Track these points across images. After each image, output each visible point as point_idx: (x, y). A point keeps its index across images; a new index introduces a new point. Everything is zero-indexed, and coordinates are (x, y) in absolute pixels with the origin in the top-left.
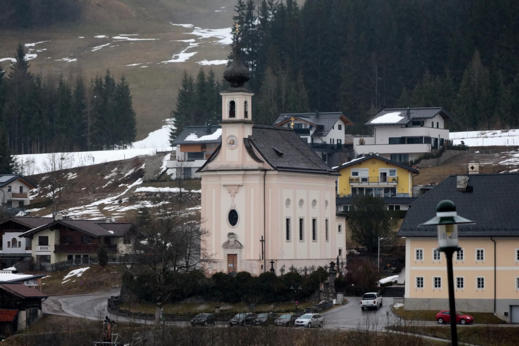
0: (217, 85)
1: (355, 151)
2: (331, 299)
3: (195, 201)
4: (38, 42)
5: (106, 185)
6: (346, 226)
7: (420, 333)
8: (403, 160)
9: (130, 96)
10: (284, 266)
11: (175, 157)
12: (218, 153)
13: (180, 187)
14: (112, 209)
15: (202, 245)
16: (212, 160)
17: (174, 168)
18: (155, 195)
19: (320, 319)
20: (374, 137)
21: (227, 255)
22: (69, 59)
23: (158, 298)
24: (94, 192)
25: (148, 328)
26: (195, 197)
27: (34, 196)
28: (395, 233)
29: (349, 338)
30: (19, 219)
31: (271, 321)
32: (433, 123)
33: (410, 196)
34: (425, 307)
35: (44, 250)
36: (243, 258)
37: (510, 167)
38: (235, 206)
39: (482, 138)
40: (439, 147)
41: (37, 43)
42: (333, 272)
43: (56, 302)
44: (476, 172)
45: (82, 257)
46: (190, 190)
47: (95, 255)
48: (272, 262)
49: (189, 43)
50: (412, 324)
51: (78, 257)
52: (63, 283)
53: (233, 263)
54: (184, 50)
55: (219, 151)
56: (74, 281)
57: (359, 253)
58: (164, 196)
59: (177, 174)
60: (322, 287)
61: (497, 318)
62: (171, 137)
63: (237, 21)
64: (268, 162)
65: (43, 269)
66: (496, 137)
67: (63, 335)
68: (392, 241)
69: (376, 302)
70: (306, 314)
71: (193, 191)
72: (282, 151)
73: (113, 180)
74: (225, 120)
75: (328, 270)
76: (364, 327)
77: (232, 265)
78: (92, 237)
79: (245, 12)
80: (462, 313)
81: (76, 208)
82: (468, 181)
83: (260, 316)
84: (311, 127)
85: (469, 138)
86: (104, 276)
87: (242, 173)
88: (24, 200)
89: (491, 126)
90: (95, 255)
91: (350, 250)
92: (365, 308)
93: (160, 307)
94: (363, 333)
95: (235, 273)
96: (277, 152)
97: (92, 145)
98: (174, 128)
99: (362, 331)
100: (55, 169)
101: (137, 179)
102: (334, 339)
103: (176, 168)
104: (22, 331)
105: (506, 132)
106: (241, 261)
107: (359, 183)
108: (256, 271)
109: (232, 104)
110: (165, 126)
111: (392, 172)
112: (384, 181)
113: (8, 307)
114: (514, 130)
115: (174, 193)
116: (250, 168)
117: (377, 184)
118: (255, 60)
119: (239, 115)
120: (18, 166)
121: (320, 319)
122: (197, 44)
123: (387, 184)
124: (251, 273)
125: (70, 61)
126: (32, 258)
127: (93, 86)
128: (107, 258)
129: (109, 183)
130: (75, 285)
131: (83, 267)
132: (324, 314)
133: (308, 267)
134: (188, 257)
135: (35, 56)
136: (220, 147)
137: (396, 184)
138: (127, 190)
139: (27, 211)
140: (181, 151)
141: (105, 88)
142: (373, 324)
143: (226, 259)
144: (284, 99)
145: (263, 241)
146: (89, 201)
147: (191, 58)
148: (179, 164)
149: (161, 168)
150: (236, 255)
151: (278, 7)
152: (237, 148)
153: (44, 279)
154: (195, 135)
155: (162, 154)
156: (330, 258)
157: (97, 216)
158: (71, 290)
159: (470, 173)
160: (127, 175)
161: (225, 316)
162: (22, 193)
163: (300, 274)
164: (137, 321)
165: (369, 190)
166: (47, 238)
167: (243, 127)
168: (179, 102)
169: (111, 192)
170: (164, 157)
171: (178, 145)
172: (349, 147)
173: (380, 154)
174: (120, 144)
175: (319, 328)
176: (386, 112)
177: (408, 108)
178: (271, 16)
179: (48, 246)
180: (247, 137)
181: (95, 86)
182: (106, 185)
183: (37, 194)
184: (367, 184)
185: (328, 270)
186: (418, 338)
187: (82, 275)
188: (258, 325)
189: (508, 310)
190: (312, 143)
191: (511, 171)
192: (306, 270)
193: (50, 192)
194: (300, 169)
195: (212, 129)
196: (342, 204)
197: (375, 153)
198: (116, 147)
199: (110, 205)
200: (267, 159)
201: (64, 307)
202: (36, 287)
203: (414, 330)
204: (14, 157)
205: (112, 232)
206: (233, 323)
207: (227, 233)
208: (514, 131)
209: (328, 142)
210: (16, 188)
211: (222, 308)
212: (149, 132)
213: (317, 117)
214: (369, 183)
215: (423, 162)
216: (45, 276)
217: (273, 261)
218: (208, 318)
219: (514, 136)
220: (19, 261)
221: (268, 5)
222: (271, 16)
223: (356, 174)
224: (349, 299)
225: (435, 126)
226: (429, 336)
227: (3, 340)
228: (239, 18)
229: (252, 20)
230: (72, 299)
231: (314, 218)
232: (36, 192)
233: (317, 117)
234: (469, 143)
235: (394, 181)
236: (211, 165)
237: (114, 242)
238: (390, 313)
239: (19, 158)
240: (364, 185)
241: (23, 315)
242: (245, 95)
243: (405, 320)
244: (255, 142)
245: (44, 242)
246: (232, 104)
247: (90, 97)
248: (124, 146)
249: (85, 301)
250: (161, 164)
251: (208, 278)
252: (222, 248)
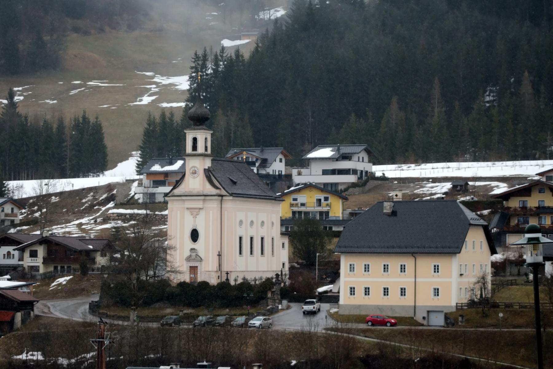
0: (176, 123)
1: (294, 181)
2: (277, 305)
3: (158, 221)
4: (24, 86)
5: (84, 207)
6: (289, 244)
7: (353, 334)
8: (334, 189)
9: (102, 132)
10: (238, 276)
11: (142, 184)
12: (182, 181)
13: (146, 209)
14: (89, 227)
15: (168, 258)
16: (178, 187)
17: (141, 193)
18: (125, 216)
19: (270, 321)
20: (310, 169)
21: (189, 267)
22: (50, 100)
23: (133, 303)
24: (74, 213)
25: (124, 328)
26: (158, 218)
27: (23, 216)
28: (330, 250)
29: (294, 337)
30: (12, 235)
31: (228, 322)
32: (359, 157)
33: (341, 219)
34: (356, 312)
35: (34, 261)
36: (203, 270)
37: (424, 195)
38: (196, 226)
39: (400, 171)
40: (364, 178)
41: (23, 87)
42: (278, 282)
43: (45, 306)
44: (400, 199)
45: (66, 267)
46: (155, 212)
47: (77, 266)
48: (227, 273)
49: (151, 88)
50: (347, 326)
51: (62, 267)
52: (50, 289)
53: (194, 274)
54: (147, 94)
55: (183, 180)
56: (60, 288)
57: (299, 266)
58: (132, 217)
59: (143, 198)
60: (269, 295)
61: (416, 321)
62: (138, 167)
63: (193, 70)
64: (224, 188)
65: (33, 278)
66: (410, 170)
67: (54, 333)
68: (327, 256)
69: (315, 307)
70: (258, 317)
71: (157, 213)
72: (236, 179)
73: (89, 203)
74: (189, 153)
75: (274, 280)
76: (307, 329)
77: (193, 276)
78: (75, 251)
79: (200, 63)
80: (387, 316)
81: (59, 226)
82: (393, 206)
83: (219, 318)
84: (257, 160)
85: (388, 170)
86: (84, 284)
87: (203, 198)
88: (14, 219)
89: (406, 161)
90: (77, 266)
91: (292, 264)
92: (306, 313)
93: (134, 310)
94: (307, 334)
95: (196, 282)
96: (232, 180)
97: (70, 173)
98: (139, 159)
99: (305, 331)
100: (42, 193)
101: (110, 203)
102: (281, 338)
103: (143, 193)
104: (18, 330)
105: (419, 166)
106: (201, 273)
107: (298, 207)
108: (213, 281)
109: (195, 140)
110: (131, 158)
111: (326, 199)
112: (319, 206)
113: (6, 309)
114: (425, 164)
115: (141, 215)
116: (209, 194)
117: (313, 208)
118: (208, 103)
119: (201, 149)
120: (10, 191)
121: (270, 321)
122: (158, 89)
123: (321, 208)
124: (209, 282)
125: (51, 102)
126: (24, 268)
127: (72, 123)
128: (88, 269)
129: (86, 205)
130: (61, 291)
131: (67, 276)
132: (272, 316)
133: (257, 278)
134: (155, 268)
135: (22, 98)
136: (184, 176)
137: (329, 208)
138: (101, 212)
139: (18, 228)
140: (147, 179)
141: (82, 125)
142: (315, 326)
143: (189, 271)
144: (232, 136)
145: (219, 255)
146: (69, 220)
147: (153, 101)
148: (146, 189)
149: (130, 193)
150: (197, 267)
151: (228, 59)
152: (198, 178)
153: (35, 285)
154: (159, 165)
155: (130, 182)
156: (275, 270)
157: (76, 234)
158: (57, 295)
159: (394, 200)
160: (101, 199)
161: (189, 318)
162: (13, 214)
163: (251, 283)
164: (116, 322)
165: (306, 213)
166: (36, 251)
167: (204, 160)
168: (144, 138)
169: (88, 213)
170: (132, 184)
171: (144, 174)
172: (289, 177)
173: (316, 183)
174: (94, 173)
175: (269, 329)
176: (320, 148)
177: (339, 145)
178: (221, 67)
179: (37, 258)
180: (207, 168)
181: (74, 124)
182: (84, 207)
183: (25, 215)
184: (305, 208)
185: (274, 280)
186: (352, 337)
187: (67, 282)
188: (217, 326)
189: (425, 315)
190: (258, 174)
191: (424, 199)
192: (255, 280)
193: (37, 212)
194: (247, 195)
195: (173, 161)
196: (285, 225)
197: (311, 182)
198: (90, 175)
199: (87, 224)
200: (223, 186)
201: (52, 310)
202: (28, 293)
203: (349, 331)
204: (6, 183)
205: (91, 247)
206: (196, 324)
207: (190, 248)
208: (426, 165)
209: (271, 173)
210: (8, 209)
211: (185, 312)
212: (118, 163)
213: (262, 151)
214: (306, 207)
215: (351, 190)
216: (36, 283)
217: (228, 272)
218: (174, 320)
219: (425, 169)
220: (13, 270)
221: (220, 58)
222: (221, 67)
223: (295, 200)
224: (292, 304)
225: (361, 160)
226: (361, 336)
227: (2, 337)
228: (196, 68)
229: (206, 70)
230: (58, 303)
231: (241, 236)
232: (25, 213)
233: (262, 151)
234: (389, 175)
235: (328, 206)
236: (177, 191)
237: (93, 254)
238: (328, 317)
239: (10, 184)
240: (303, 209)
241: (19, 316)
242: (206, 133)
243: (341, 322)
244: (213, 173)
245: (34, 254)
246: (195, 140)
247: (70, 133)
248: (97, 175)
249: (70, 304)
250: (130, 190)
251: (173, 286)
252: (185, 261)
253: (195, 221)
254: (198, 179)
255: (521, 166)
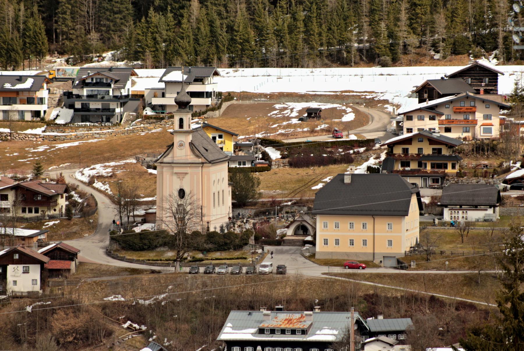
34: (340, 258)
48: (208, 223)
109: (181, 120)
246: (181, 120)
253: (181, 183)
254: (184, 151)
255: (333, 76)
